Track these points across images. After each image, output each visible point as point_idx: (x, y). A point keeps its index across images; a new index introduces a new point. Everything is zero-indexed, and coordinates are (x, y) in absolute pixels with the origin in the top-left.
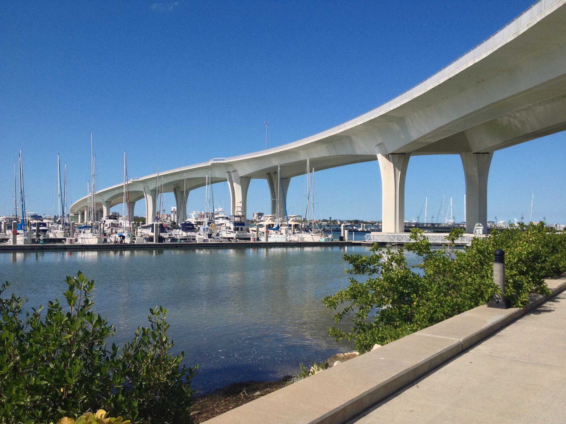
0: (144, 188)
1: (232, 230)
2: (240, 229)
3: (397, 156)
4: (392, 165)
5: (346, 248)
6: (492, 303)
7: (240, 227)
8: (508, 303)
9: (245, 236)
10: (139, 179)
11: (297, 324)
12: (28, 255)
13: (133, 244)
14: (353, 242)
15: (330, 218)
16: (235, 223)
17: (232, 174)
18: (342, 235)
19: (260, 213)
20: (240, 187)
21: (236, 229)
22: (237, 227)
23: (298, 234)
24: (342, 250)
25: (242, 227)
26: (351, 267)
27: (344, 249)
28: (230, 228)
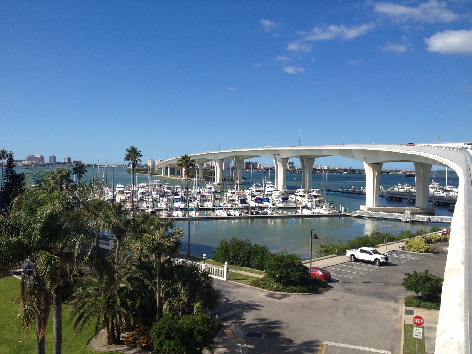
0: (214, 158)
1: (281, 202)
2: (285, 201)
3: (374, 165)
4: (372, 168)
5: (343, 218)
6: (336, 254)
7: (285, 200)
8: (338, 254)
9: (288, 206)
10: (211, 152)
11: (84, 206)
12: (200, 221)
13: (241, 216)
14: (347, 214)
15: (351, 167)
16: (283, 198)
17: (277, 156)
18: (341, 211)
19: (291, 162)
20: (282, 165)
21: (283, 202)
22: (284, 200)
23: (318, 209)
24: (341, 219)
25: (286, 200)
26: (320, 247)
27: (342, 218)
28: (280, 201)
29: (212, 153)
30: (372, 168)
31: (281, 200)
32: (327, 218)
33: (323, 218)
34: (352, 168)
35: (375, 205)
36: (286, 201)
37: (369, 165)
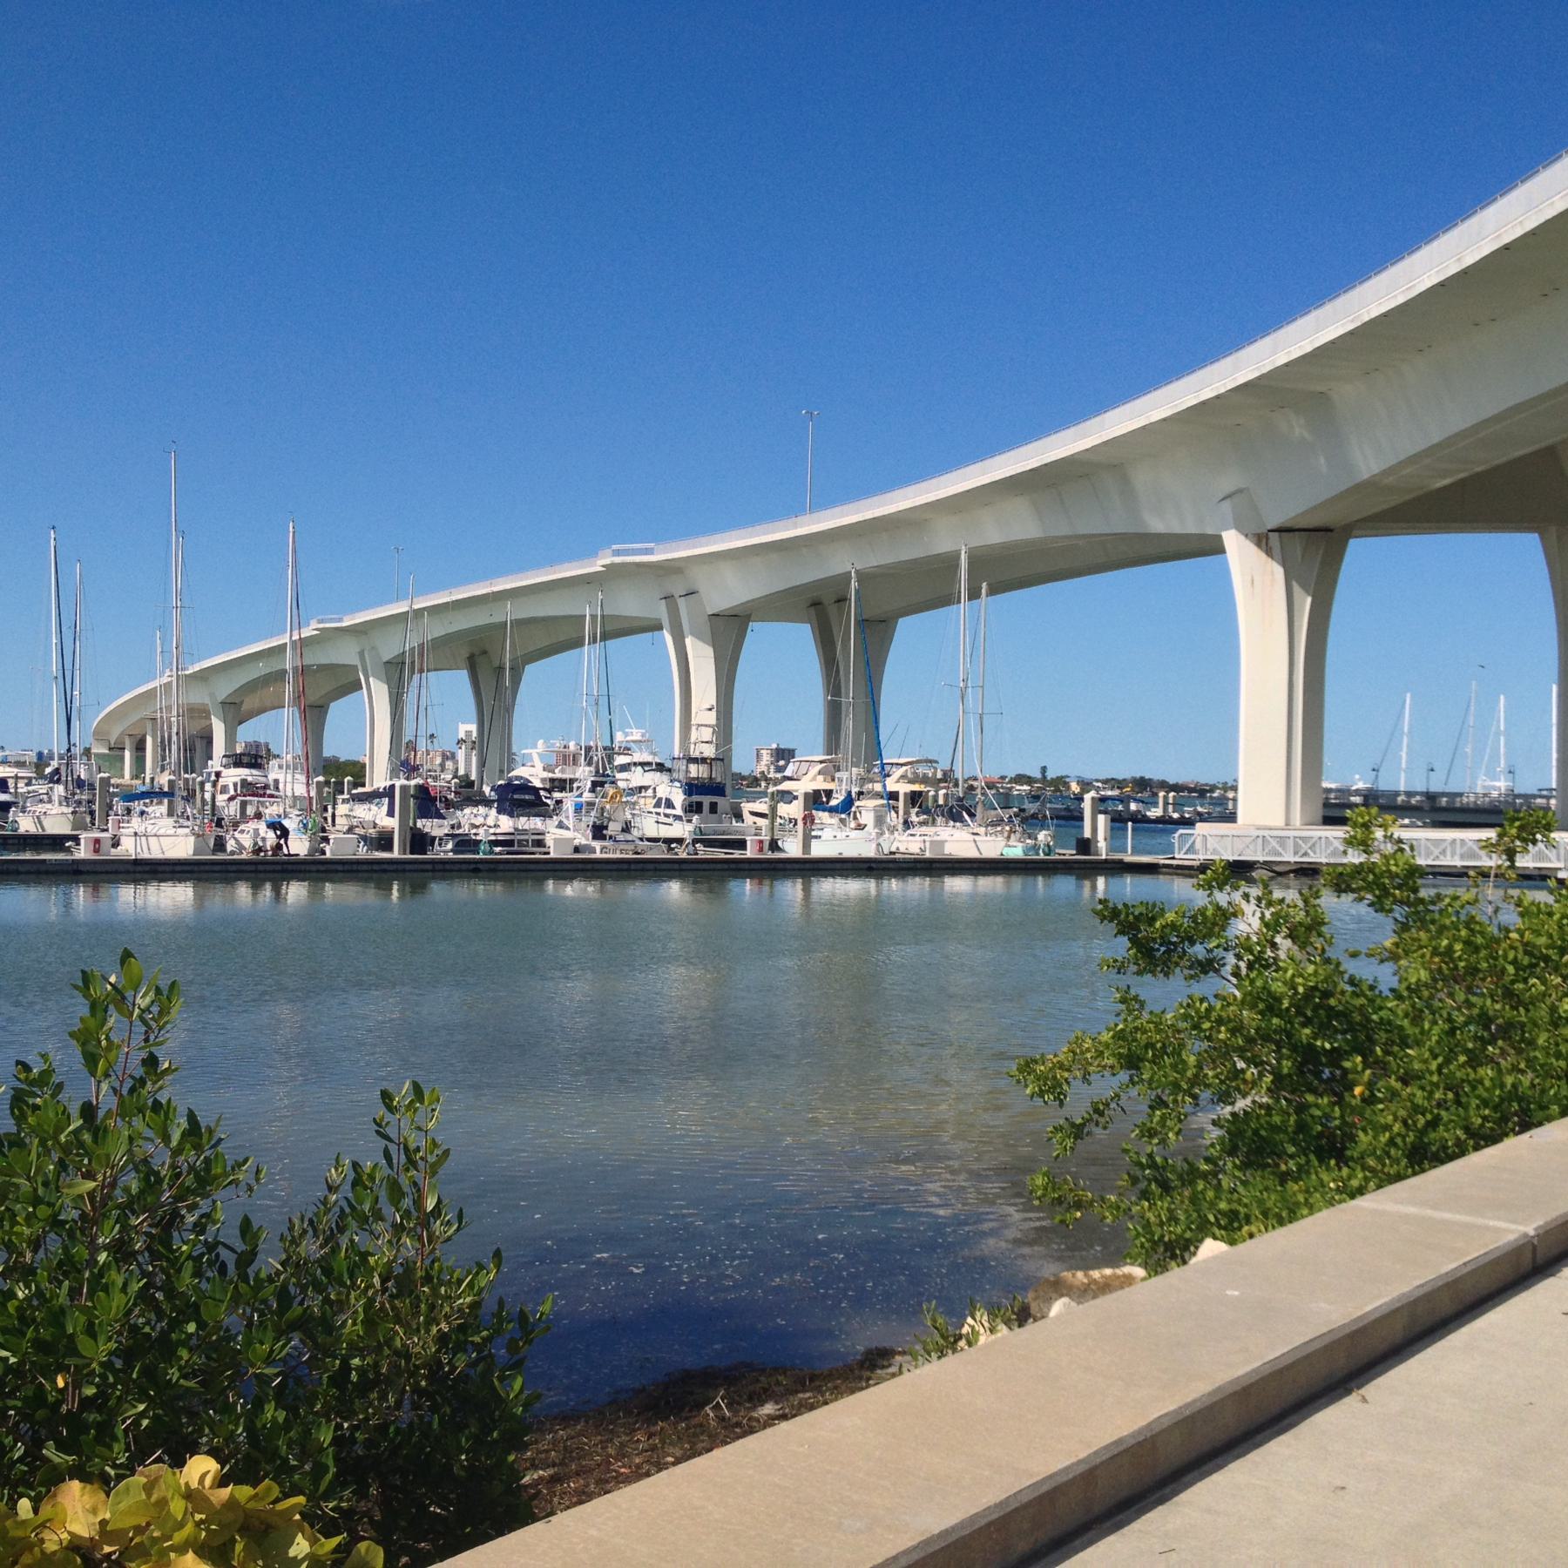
1: (679, 811)
2: (706, 807)
3: (1296, 542)
4: (1279, 571)
7: (706, 800)
10: (340, 620)
14: (1129, 858)
15: (1044, 769)
17: (682, 603)
18: (1087, 834)
19: (783, 750)
21: (693, 808)
22: (696, 798)
23: (924, 829)
28: (669, 804)
29: (344, 624)
30: (1284, 565)
31: (678, 798)
32: (991, 884)
33: (958, 885)
34: (1050, 775)
35: (1301, 820)
36: (713, 808)
37: (1261, 540)
